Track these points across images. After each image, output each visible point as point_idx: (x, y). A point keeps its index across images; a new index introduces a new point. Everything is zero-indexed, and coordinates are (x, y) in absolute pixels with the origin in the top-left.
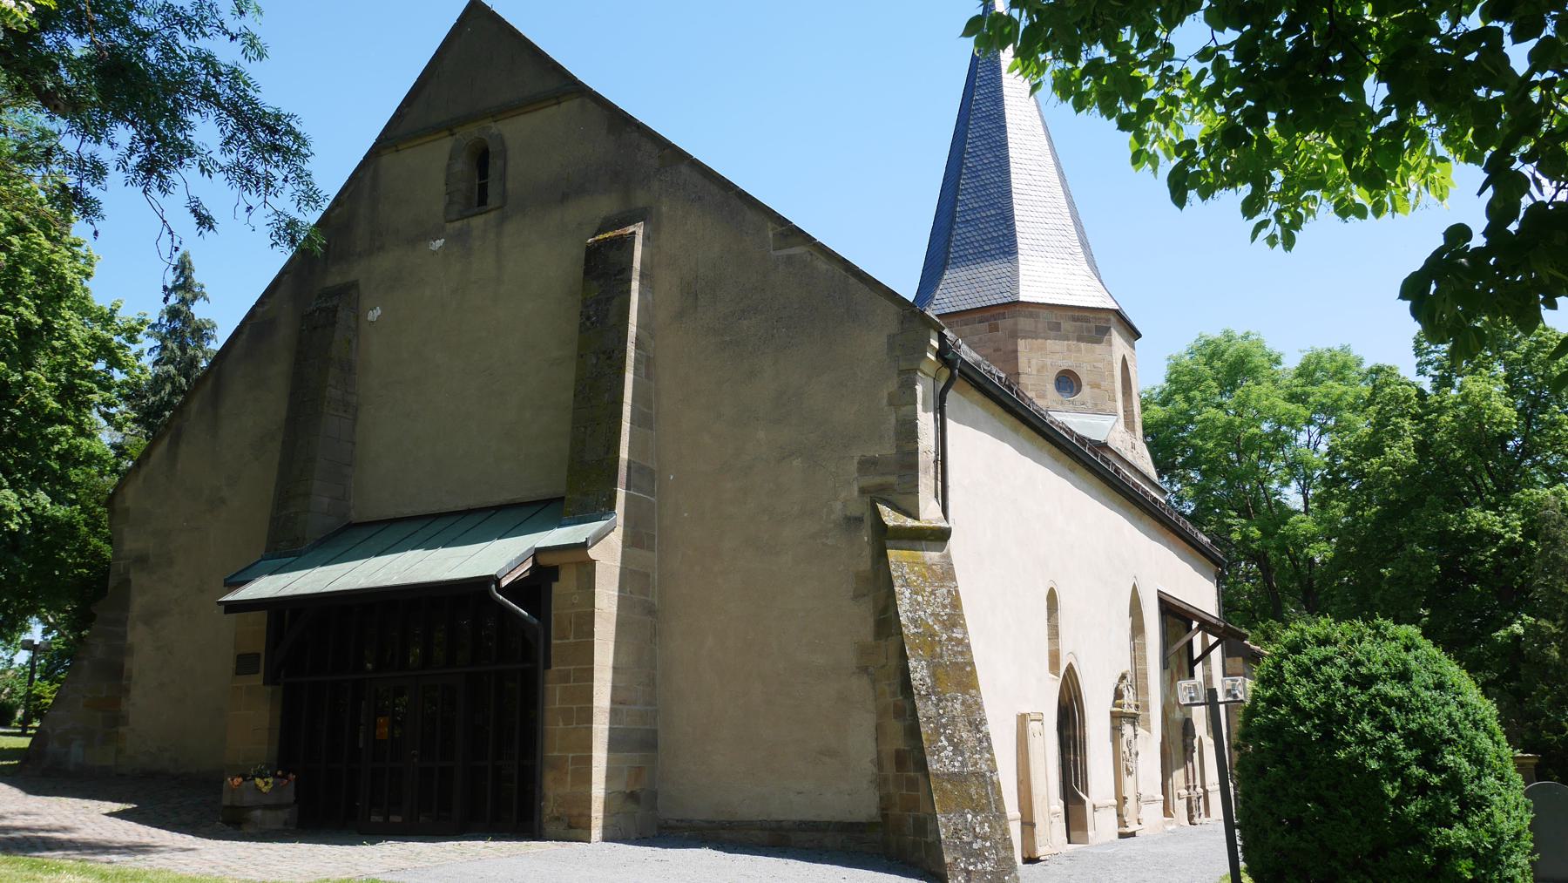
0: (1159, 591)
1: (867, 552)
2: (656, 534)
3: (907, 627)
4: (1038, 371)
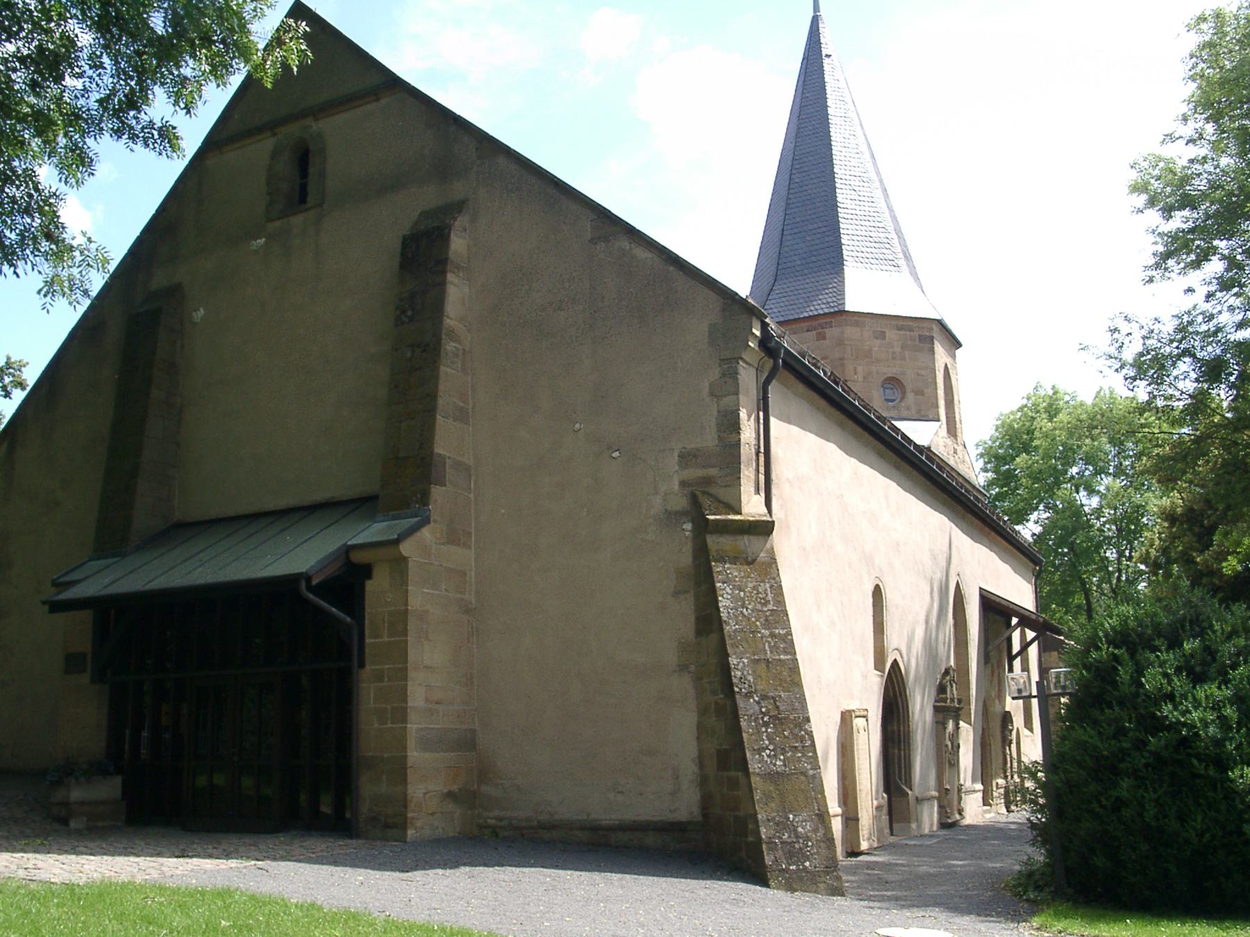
0: (980, 588)
1: (688, 549)
2: (473, 531)
3: (728, 624)
4: (864, 378)
